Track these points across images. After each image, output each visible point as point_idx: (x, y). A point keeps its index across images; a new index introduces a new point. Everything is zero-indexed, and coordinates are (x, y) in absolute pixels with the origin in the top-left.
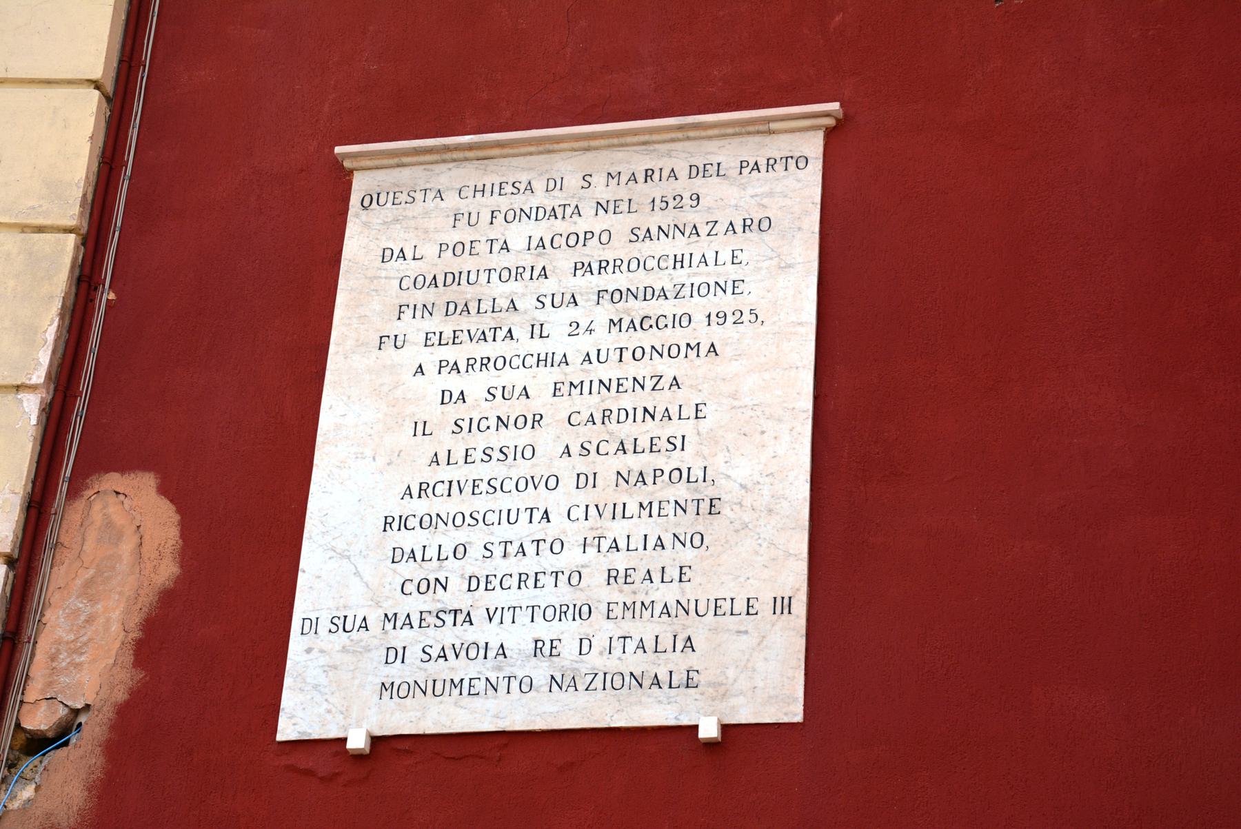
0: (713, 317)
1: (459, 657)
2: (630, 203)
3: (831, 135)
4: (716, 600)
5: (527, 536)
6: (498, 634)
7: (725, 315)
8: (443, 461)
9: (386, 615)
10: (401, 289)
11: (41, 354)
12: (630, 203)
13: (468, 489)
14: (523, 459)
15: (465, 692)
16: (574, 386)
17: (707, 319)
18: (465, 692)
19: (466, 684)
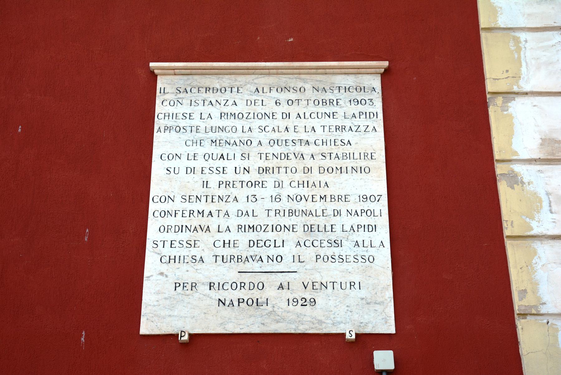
0: (291, 301)
1: (351, 226)
2: (219, 215)
3: (386, 75)
4: (266, 153)
5: (344, 84)
6: (388, 267)
7: (298, 301)
8: (310, 198)
9: (212, 141)
10: (236, 173)
11: (523, 321)
12: (219, 215)
13: (310, 199)
14: (279, 209)
15: (218, 144)
16: (322, 198)
17: (288, 301)
18: (218, 144)
19: (218, 142)
